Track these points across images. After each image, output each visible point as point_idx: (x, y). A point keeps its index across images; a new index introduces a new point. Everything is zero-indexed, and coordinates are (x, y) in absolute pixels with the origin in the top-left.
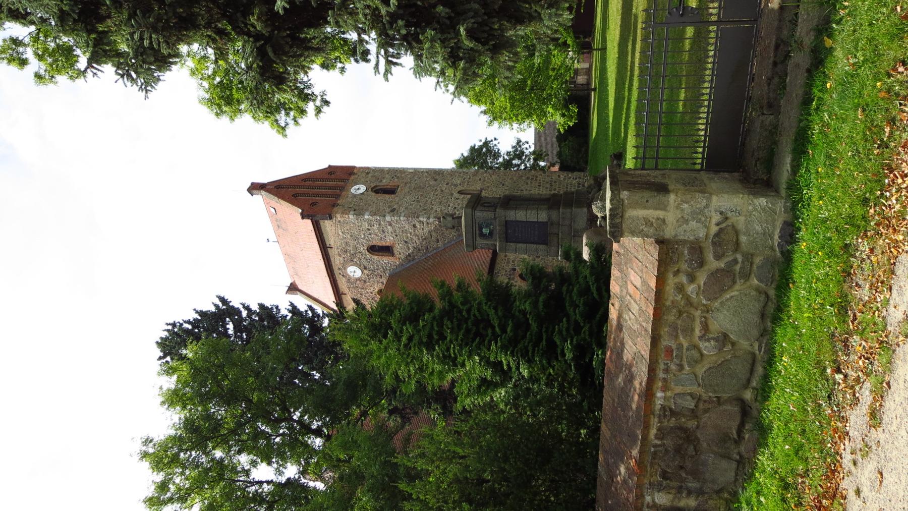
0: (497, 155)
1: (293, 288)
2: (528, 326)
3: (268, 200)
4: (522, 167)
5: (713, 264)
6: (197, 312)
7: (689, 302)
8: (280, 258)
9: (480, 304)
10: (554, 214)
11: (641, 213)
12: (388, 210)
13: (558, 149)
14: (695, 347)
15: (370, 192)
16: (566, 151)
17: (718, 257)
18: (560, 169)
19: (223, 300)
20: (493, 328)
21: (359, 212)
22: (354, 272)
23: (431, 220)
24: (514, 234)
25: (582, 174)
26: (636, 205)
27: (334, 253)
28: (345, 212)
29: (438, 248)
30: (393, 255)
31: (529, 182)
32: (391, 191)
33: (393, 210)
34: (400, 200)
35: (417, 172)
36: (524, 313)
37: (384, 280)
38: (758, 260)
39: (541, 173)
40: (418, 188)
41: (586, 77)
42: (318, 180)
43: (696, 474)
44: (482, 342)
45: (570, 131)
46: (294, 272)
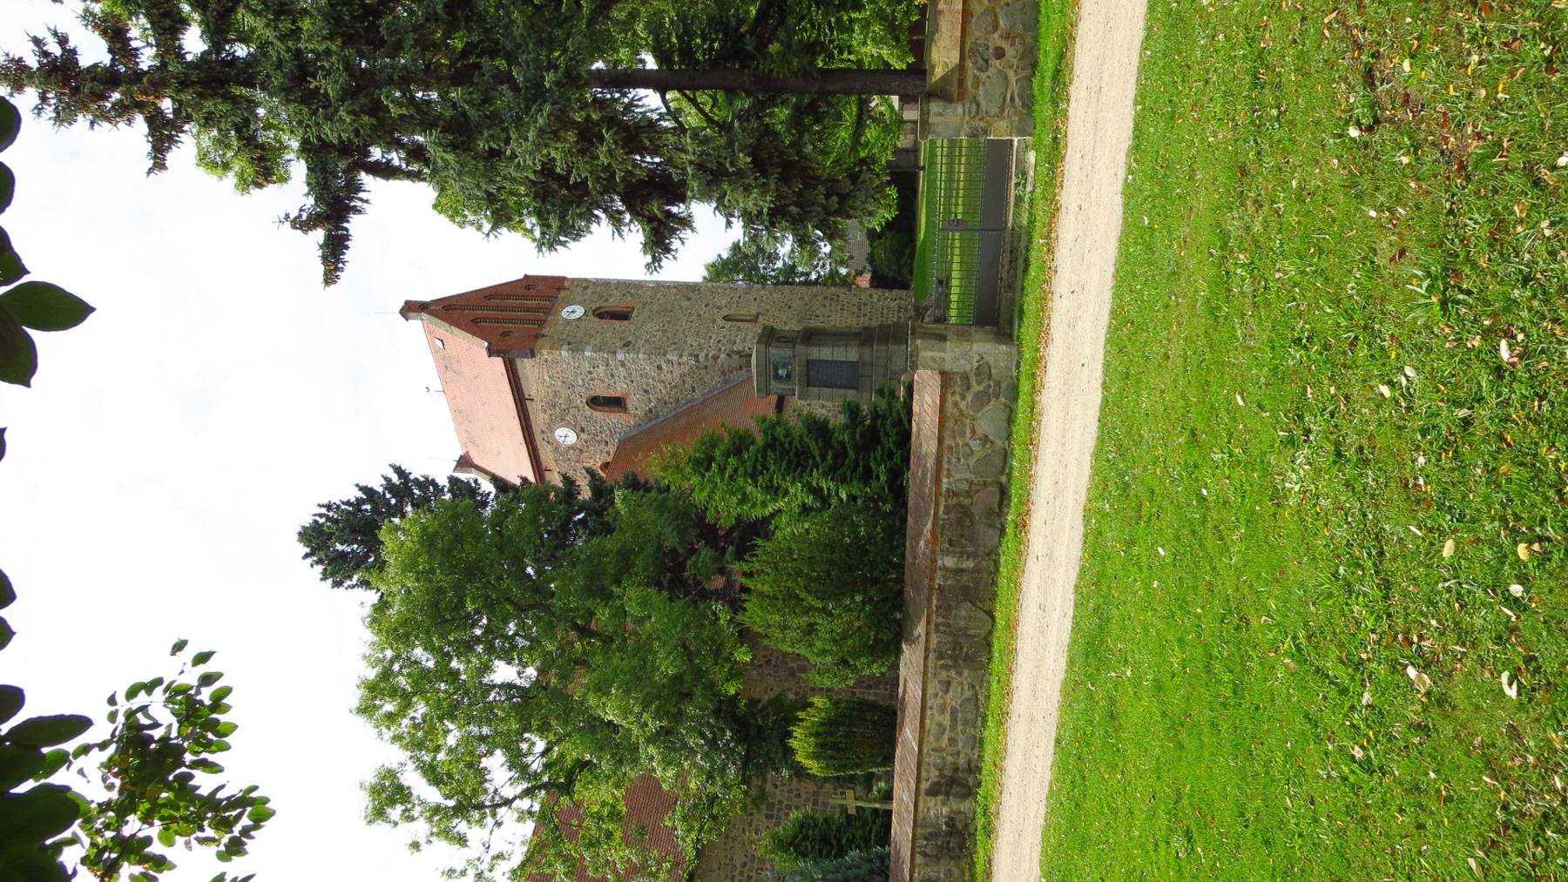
1: (464, 462)
2: (845, 454)
5: (976, 388)
9: (801, 436)
10: (867, 352)
11: (929, 354)
12: (619, 344)
15: (591, 317)
16: (881, 254)
17: (979, 383)
19: (399, 471)
21: (576, 347)
22: (566, 436)
23: (685, 358)
24: (816, 377)
26: (925, 349)
30: (625, 410)
32: (623, 316)
33: (627, 344)
36: (842, 444)
37: (612, 449)
38: (1003, 385)
40: (664, 311)
42: (509, 297)
43: (972, 540)
46: (466, 435)
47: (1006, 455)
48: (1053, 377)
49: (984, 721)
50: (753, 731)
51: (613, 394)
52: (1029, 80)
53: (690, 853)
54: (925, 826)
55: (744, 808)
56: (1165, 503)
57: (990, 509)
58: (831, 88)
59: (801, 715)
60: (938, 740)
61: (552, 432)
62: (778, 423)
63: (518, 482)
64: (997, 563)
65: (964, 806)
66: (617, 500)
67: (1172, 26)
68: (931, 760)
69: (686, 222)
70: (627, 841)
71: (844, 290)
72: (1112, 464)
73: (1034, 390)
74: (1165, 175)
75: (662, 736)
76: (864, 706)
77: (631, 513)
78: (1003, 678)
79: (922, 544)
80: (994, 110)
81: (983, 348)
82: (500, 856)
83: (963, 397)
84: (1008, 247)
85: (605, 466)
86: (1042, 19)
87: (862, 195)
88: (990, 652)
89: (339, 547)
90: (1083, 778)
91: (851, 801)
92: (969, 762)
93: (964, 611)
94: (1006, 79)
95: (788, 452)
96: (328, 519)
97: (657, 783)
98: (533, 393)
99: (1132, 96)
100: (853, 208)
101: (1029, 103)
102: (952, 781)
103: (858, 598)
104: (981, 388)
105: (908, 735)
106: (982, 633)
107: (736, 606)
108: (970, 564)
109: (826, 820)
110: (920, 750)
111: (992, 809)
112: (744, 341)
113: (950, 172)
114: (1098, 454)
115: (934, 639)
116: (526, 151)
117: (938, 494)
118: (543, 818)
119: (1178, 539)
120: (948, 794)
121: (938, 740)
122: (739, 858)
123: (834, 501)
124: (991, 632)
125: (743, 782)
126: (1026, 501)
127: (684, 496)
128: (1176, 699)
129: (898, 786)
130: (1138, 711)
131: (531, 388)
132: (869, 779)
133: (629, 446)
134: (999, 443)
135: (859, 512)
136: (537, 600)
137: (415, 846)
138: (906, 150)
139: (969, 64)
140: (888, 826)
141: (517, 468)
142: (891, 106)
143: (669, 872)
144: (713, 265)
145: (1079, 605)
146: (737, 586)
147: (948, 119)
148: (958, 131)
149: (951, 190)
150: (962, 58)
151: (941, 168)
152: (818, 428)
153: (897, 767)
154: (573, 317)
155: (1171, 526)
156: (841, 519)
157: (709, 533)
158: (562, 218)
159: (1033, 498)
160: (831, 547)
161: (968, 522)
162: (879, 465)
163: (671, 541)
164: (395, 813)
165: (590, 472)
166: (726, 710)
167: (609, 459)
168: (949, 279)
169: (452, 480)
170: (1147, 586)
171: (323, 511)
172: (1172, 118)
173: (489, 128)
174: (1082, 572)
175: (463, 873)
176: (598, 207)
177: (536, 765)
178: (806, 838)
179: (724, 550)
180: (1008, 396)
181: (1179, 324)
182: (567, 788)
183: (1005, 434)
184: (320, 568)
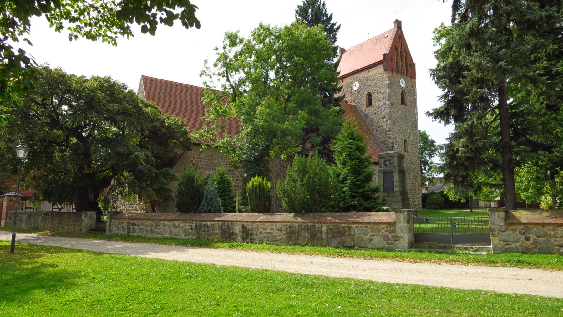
1: (343, 51)
2: (360, 188)
3: (392, 32)
5: (390, 236)
6: (331, 15)
7: (380, 231)
9: (365, 172)
10: (398, 194)
12: (392, 102)
13: (436, 192)
14: (368, 233)
17: (392, 236)
18: (424, 194)
19: (339, 28)
20: (358, 177)
21: (390, 86)
22: (356, 86)
23: (389, 126)
24: (387, 175)
25: (421, 206)
27: (365, 73)
28: (389, 78)
29: (373, 131)
30: (367, 107)
31: (415, 178)
32: (403, 102)
33: (392, 105)
34: (398, 108)
36: (364, 187)
37: (353, 103)
38: (392, 246)
40: (406, 117)
41: (483, 206)
42: (406, 59)
44: (352, 173)
46: (352, 50)
47: (365, 248)
48: (397, 264)
49: (269, 244)
50: (258, 163)
51: (373, 101)
52: (518, 251)
55: (232, 162)
56: (357, 308)
57: (344, 243)
59: (265, 179)
61: (357, 81)
62: (369, 163)
63: (338, 71)
64: (325, 246)
65: (239, 238)
66: (335, 108)
67: (553, 309)
68: (254, 226)
69: (447, 122)
71: (420, 184)
72: (369, 288)
73: (392, 257)
74: (488, 307)
76: (270, 201)
79: (330, 218)
80: (503, 238)
81: (406, 238)
83: (386, 231)
84: (446, 245)
85: (346, 102)
86: (545, 255)
87: (463, 189)
88: (293, 245)
89: (310, 10)
90: (255, 280)
91: (238, 199)
92: (254, 239)
93: (307, 235)
94: (517, 242)
96: (319, 5)
98: (371, 72)
99: (518, 292)
101: (506, 251)
102: (247, 234)
103: (308, 196)
104: (390, 237)
105: (262, 217)
106: (300, 242)
107: (300, 153)
108: (324, 236)
109: (230, 191)
110: (257, 222)
111: (239, 248)
112: (397, 148)
113: (472, 222)
114: (372, 282)
115: (296, 225)
116: (472, 59)
117: (349, 223)
118: (225, 94)
119: (345, 313)
120: (243, 232)
122: (215, 161)
123: (342, 185)
124: (300, 245)
125: (241, 161)
126: (350, 256)
127: (339, 131)
129: (245, 214)
130: (280, 299)
131: (372, 71)
132: (245, 204)
133: (354, 109)
134: (370, 245)
135: (339, 194)
136: (297, 82)
138: (478, 204)
139: (522, 227)
140: (230, 212)
141: (343, 69)
142: (496, 197)
143: (210, 137)
144: (425, 134)
145: (315, 277)
146: (308, 153)
147: (498, 219)
148: (493, 224)
149: (465, 222)
150: (524, 224)
151: (473, 218)
152: (369, 178)
155: (349, 311)
156: (336, 189)
157: (327, 140)
158: (443, 77)
159: (351, 259)
160: (326, 185)
161: (339, 235)
163: (323, 128)
164: (227, 42)
165: (344, 96)
167: (349, 103)
168: (429, 223)
169: (337, 48)
170: (326, 302)
171: (322, 3)
172: (512, 309)
173: (480, 43)
174: (327, 278)
177: (241, 89)
178: (224, 184)
179: (320, 146)
180: (388, 247)
181: (427, 313)
183: (373, 247)
184: (302, 5)
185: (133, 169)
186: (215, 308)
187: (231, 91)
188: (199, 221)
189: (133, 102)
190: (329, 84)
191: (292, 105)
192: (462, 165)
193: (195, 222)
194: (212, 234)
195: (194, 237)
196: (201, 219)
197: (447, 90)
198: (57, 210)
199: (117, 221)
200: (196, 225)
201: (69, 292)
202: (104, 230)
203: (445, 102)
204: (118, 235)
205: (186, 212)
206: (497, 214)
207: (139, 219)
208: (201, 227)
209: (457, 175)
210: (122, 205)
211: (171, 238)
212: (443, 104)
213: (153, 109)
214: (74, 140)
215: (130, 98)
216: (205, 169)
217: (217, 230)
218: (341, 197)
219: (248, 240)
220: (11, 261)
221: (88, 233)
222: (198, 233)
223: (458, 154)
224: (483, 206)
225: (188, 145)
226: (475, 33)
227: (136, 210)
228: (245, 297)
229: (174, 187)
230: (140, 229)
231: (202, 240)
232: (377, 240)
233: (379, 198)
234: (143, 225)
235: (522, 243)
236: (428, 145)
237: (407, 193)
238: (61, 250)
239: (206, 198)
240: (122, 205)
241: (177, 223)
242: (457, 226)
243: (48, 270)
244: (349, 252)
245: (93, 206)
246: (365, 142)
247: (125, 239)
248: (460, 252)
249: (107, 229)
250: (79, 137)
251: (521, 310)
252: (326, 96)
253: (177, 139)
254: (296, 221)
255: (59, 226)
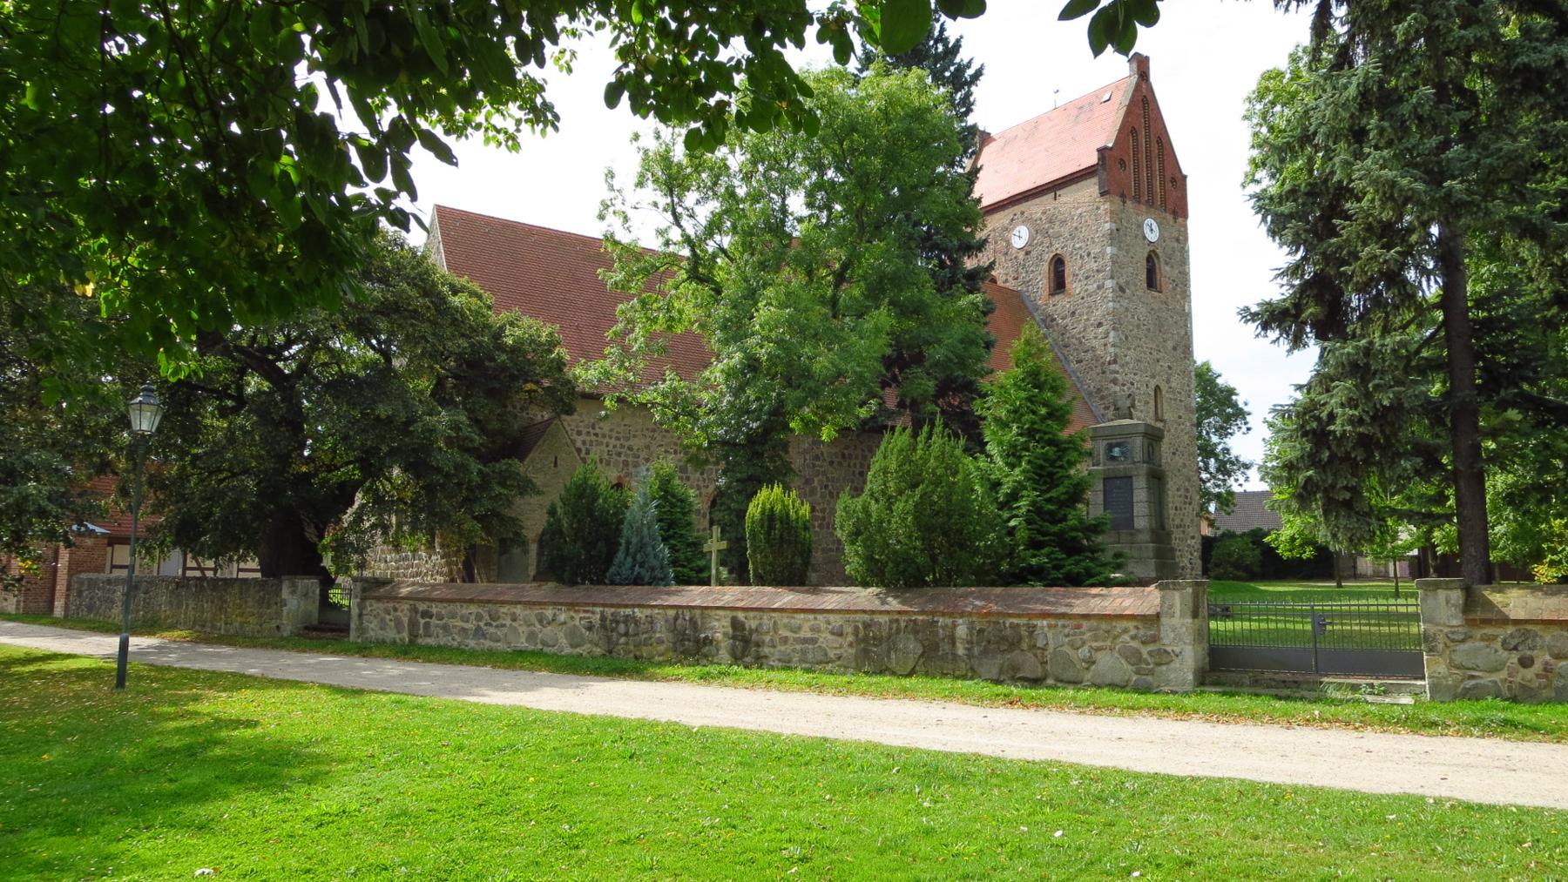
0: (1223, 431)
2: (1054, 522)
3: (1123, 87)
4: (1204, 476)
5: (1145, 651)
6: (958, 41)
7: (1115, 638)
8: (1030, 115)
9: (1069, 477)
10: (1146, 537)
12: (1122, 281)
13: (1238, 532)
14: (1084, 643)
17: (1150, 653)
19: (978, 74)
20: (1048, 490)
21: (1115, 237)
22: (1020, 237)
23: (1112, 350)
26: (1182, 598)
30: (1052, 294)
31: (1182, 492)
32: (1151, 282)
33: (1122, 289)
35: (1185, 317)
36: (1065, 518)
37: (1011, 285)
38: (1149, 678)
39: (1197, 509)
40: (1160, 324)
41: (1370, 572)
42: (1162, 162)
43: (985, 652)
45: (1269, 552)
46: (1010, 138)
47: (1076, 683)
49: (807, 671)
50: (759, 449)
53: (643, 397)
54: (703, 617)
57: (1021, 670)
58: (1462, 484)
60: (785, 626)
63: (975, 195)
64: (964, 677)
65: (724, 654)
66: (971, 297)
68: (765, 621)
69: (1297, 342)
70: (651, 337)
73: (1152, 709)
75: (752, 364)
76: (806, 553)
77: (960, 313)
78: (854, 687)
80: (1458, 659)
81: (1188, 658)
82: (626, 219)
83: (1133, 638)
84: (1300, 679)
85: (994, 281)
93: (914, 647)
95: (1052, 465)
97: (707, 365)
98: (1062, 199)
100: (1337, 518)
101: (1473, 694)
102: (746, 641)
105: (786, 598)
106: (893, 665)
108: (961, 651)
109: (689, 524)
110: (774, 610)
111: (727, 680)
113: (1350, 615)
115: (883, 619)
116: (1371, 170)
117: (1030, 616)
120: (734, 637)
121: (785, 626)
122: (637, 443)
123: (1006, 515)
124: (893, 673)
128: (925, 848)
131: (1068, 196)
133: (1018, 304)
134: (1088, 676)
135: (1000, 538)
136: (865, 226)
137: (636, 137)
138: (1355, 567)
139: (1510, 630)
141: (988, 190)
143: (626, 380)
144: (1209, 370)
145: (966, 758)
150: (1516, 622)
151: (1347, 605)
152: (1076, 494)
153: (754, 589)
154: (1147, 230)
160: (965, 512)
161: (1003, 647)
162: (1048, 556)
165: (991, 266)
166: (777, 418)
167: (1000, 283)
175: (611, 188)
176: (1307, 251)
178: (673, 505)
180: (1140, 683)
182: (694, 275)
183: (1098, 681)
185: (418, 467)
186: (726, 834)
187: (686, 252)
188: (612, 606)
189: (422, 280)
190: (952, 228)
191: (853, 292)
192: (1347, 457)
193: (598, 609)
194: (646, 643)
195: (598, 651)
196: (615, 601)
197: (1301, 253)
198: (198, 574)
199: (381, 606)
200: (603, 619)
201: (317, 791)
202: (343, 629)
203: (1292, 286)
204: (384, 642)
205: (573, 583)
206: (1442, 594)
207: (442, 601)
208: (618, 622)
209: (1333, 487)
210: (382, 561)
211: (533, 653)
212: (1287, 292)
213: (474, 300)
214: (254, 383)
215: (413, 268)
216: (608, 464)
217: (662, 632)
218: (1004, 545)
219: (748, 659)
220: (128, 710)
221: (299, 635)
222: (609, 639)
223: (1332, 428)
224: (1370, 572)
225: (567, 398)
226: (1375, 98)
227: (418, 574)
228: (798, 808)
229: (533, 516)
230: (445, 628)
231: (620, 657)
232: (1109, 663)
233: (1102, 550)
234: (453, 616)
235: (1510, 675)
236: (1220, 405)
237: (1169, 534)
238: (239, 681)
239: (628, 543)
240: (382, 561)
241: (549, 612)
242: (1329, 627)
243: (236, 733)
244: (1033, 693)
245: (308, 563)
246: (1068, 396)
247: (406, 653)
248: (1338, 695)
249: (353, 626)
250: (271, 373)
251: (1542, 845)
252: (942, 265)
253: (537, 383)
254: (886, 607)
255: (216, 616)
